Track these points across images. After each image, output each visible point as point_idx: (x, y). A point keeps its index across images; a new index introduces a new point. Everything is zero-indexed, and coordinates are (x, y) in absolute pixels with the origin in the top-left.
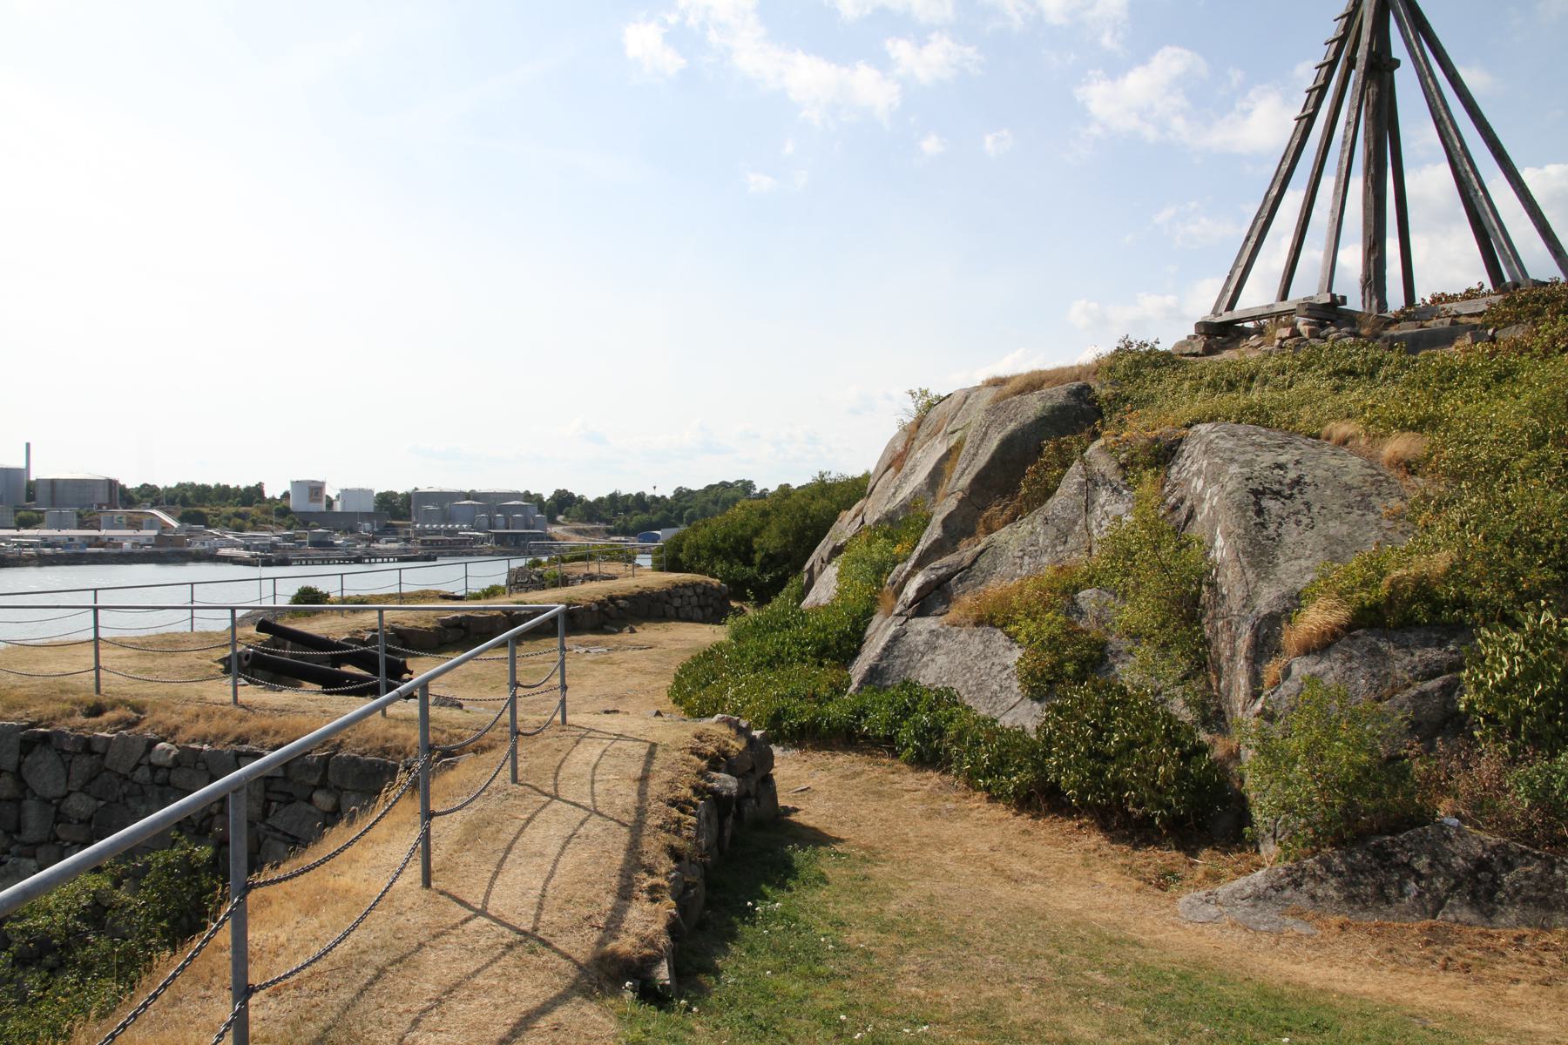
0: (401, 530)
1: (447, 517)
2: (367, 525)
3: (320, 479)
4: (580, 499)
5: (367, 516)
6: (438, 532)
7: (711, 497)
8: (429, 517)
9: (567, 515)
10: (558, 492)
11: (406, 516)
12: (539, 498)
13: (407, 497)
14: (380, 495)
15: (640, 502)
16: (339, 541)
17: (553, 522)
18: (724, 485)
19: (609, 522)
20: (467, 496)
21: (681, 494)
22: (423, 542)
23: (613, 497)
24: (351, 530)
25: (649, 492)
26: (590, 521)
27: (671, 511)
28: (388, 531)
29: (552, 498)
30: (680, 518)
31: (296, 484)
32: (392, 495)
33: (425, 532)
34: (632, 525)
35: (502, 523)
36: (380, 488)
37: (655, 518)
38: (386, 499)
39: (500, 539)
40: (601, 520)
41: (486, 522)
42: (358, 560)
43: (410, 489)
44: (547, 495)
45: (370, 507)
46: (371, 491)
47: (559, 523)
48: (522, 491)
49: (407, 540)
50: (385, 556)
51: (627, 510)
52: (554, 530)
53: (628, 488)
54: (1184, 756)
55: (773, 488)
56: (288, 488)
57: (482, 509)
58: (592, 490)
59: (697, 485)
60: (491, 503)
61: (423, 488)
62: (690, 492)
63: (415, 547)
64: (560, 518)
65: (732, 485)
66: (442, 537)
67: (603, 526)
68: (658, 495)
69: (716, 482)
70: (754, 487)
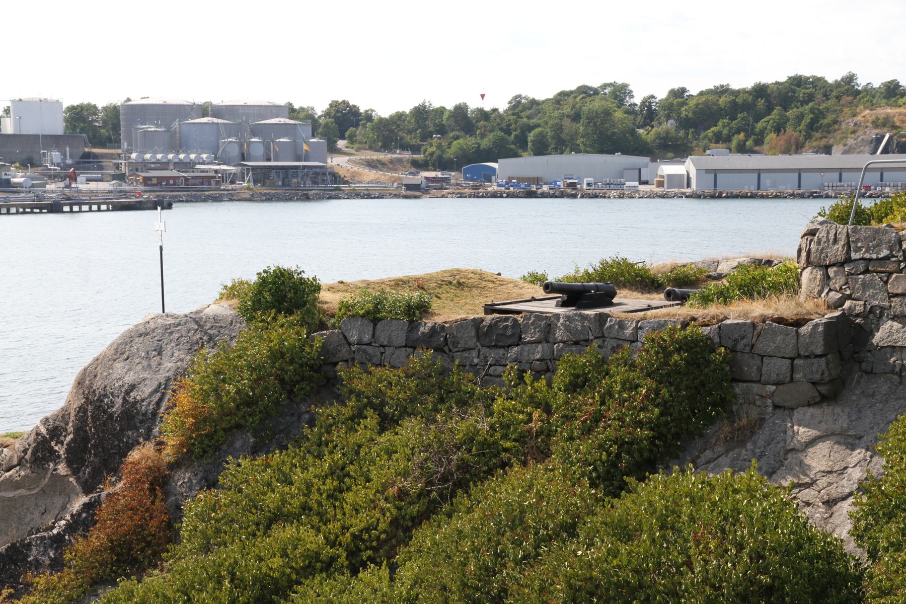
0: (106, 163)
1: (177, 143)
2: (56, 155)
3: (627, 82)
4: (368, 117)
5: (53, 141)
6: (164, 165)
7: (567, 110)
8: (148, 141)
9: (352, 139)
10: (335, 105)
11: (112, 141)
12: (306, 115)
13: (113, 112)
14: (72, 109)
15: (463, 120)
16: (18, 178)
17: (333, 150)
18: (585, 91)
19: (415, 149)
20: (204, 110)
21: (519, 106)
22: (146, 181)
23: (421, 113)
24: (28, 163)
25: (474, 104)
26: (386, 147)
27: (508, 132)
28: (87, 162)
29: (327, 114)
30: (522, 143)
31: (13, 102)
32: (91, 109)
33: (146, 166)
34: (451, 153)
35: (259, 150)
36: (72, 99)
37: (485, 143)
38: (79, 117)
39: (262, 176)
40: (404, 147)
41: (235, 151)
42: (55, 208)
43: (117, 99)
44: (320, 107)
45: (58, 127)
46: (58, 103)
47: (339, 152)
48: (282, 102)
49: (121, 177)
50: (92, 203)
51: (442, 130)
52: (337, 162)
53: (444, 98)
54: (215, 344)
55: (661, 94)
56: (9, 104)
57: (230, 131)
58: (385, 101)
59: (544, 92)
60: (240, 121)
61: (136, 101)
62: (534, 102)
63: (135, 188)
64: (341, 144)
65: (596, 92)
66: (175, 173)
67: (407, 155)
68: (487, 108)
69: (572, 87)
70: (630, 94)
